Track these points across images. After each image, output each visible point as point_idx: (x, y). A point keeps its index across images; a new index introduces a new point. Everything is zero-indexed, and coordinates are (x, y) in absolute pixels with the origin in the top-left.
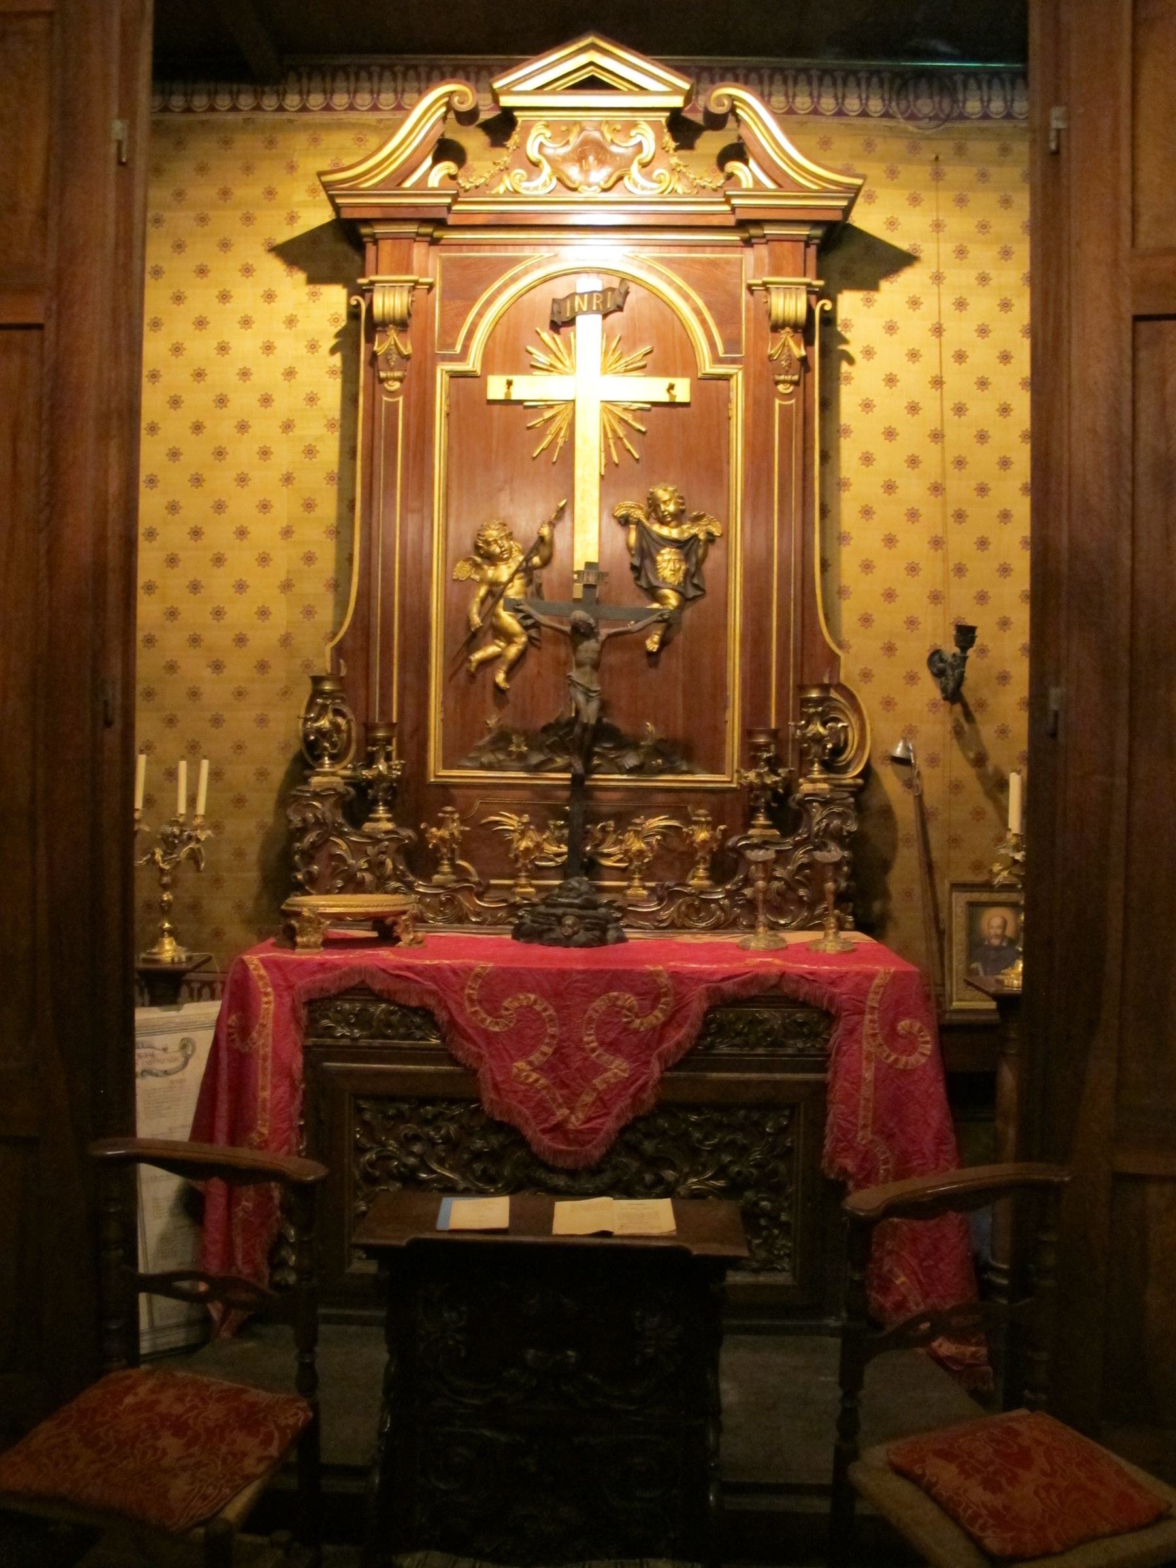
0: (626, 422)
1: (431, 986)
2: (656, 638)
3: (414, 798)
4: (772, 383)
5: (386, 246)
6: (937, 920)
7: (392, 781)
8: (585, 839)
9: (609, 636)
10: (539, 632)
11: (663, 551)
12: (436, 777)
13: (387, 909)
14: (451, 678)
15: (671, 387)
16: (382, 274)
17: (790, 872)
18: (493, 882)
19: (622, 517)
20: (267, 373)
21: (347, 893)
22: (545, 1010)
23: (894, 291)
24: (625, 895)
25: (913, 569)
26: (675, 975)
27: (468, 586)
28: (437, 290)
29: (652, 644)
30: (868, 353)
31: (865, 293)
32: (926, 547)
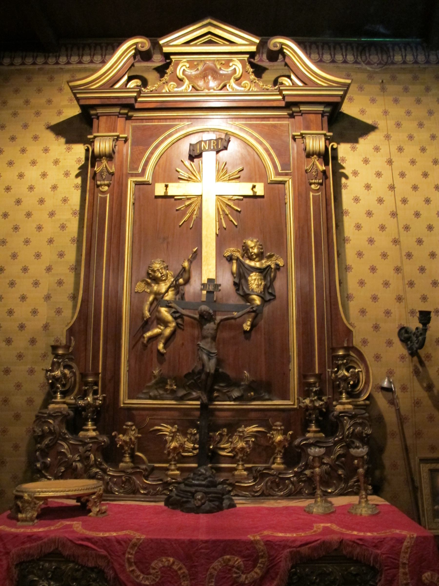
1: (103, 552)
2: (249, 323)
3: (110, 416)
4: (308, 184)
5: (103, 119)
6: (413, 481)
7: (96, 407)
8: (210, 441)
9: (222, 320)
10: (183, 320)
11: (252, 275)
12: (124, 404)
13: (82, 492)
15: (254, 187)
16: (100, 133)
17: (332, 460)
18: (157, 465)
19: (228, 256)
20: (43, 188)
21: (66, 478)
22: (180, 569)
23: (365, 144)
24: (234, 475)
25: (386, 284)
26: (269, 544)
27: (142, 295)
28: (130, 141)
29: (247, 326)
31: (352, 144)
32: (393, 272)
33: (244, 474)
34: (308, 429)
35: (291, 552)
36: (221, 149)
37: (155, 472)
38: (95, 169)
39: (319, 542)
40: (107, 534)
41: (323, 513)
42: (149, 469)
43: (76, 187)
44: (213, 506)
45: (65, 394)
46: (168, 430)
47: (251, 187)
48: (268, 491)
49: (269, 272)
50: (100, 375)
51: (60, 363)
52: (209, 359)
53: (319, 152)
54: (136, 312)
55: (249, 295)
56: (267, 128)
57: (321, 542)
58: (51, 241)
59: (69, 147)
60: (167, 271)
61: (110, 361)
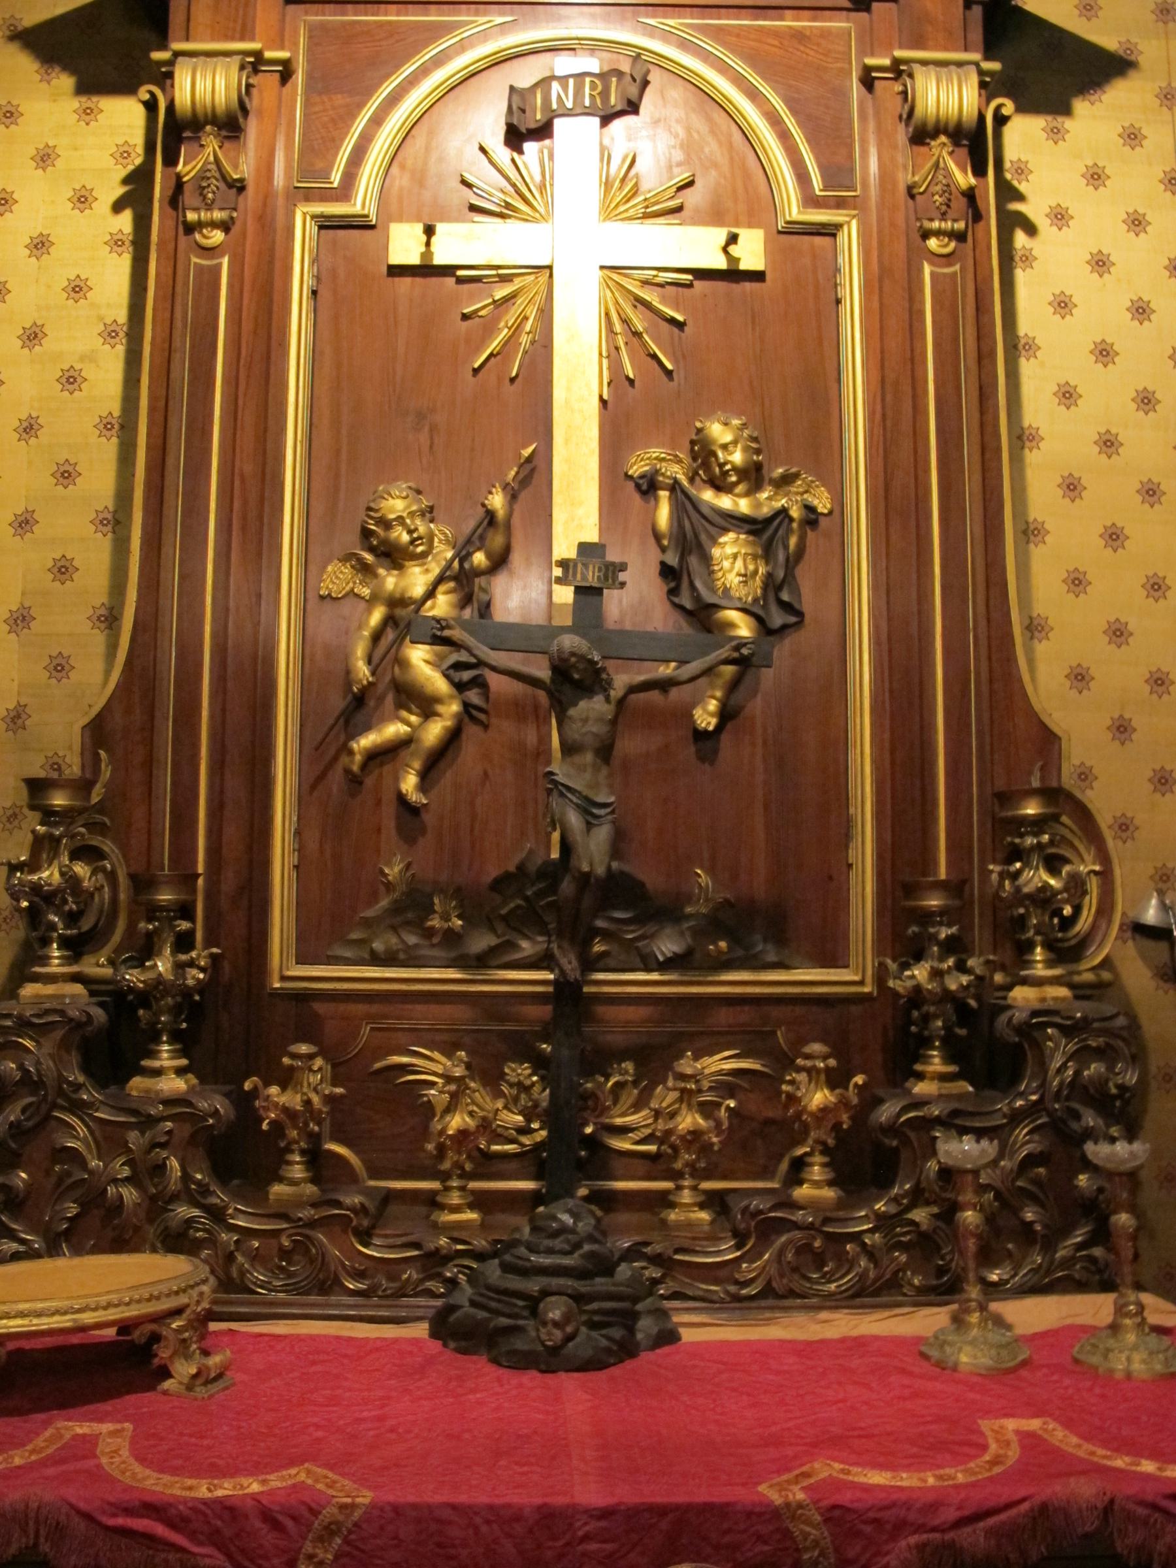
0: (647, 305)
2: (713, 705)
3: (235, 1024)
7: (186, 993)
11: (722, 540)
12: (283, 978)
14: (313, 787)
15: (733, 239)
16: (195, 40)
19: (642, 477)
23: (1094, 119)
28: (299, 77)
29: (706, 716)
30: (1060, 217)
31: (1049, 118)
33: (700, 1220)
34: (918, 1067)
35: (921, 1547)
36: (619, 108)
37: (393, 1209)
38: (180, 167)
39: (1025, 1506)
40: (225, 1489)
41: (989, 1369)
42: (371, 1206)
43: (116, 243)
44: (604, 1343)
45: (76, 948)
46: (439, 1069)
47: (723, 243)
48: (785, 1281)
49: (780, 532)
50: (200, 881)
51: (58, 840)
52: (589, 826)
53: (959, 124)
54: (323, 668)
55: (717, 607)
56: (776, 43)
57: (1032, 1509)
58: (31, 427)
59: (89, 104)
60: (432, 526)
61: (232, 833)
